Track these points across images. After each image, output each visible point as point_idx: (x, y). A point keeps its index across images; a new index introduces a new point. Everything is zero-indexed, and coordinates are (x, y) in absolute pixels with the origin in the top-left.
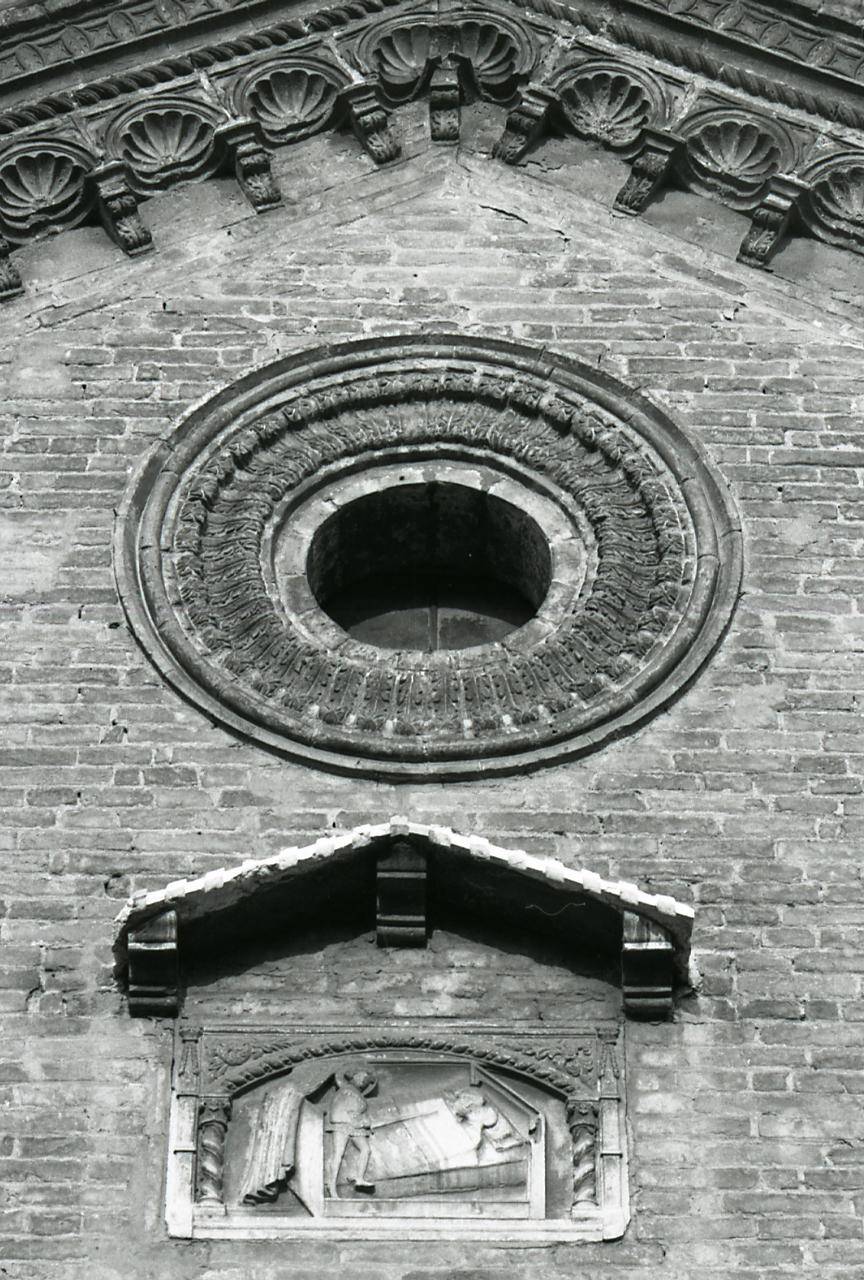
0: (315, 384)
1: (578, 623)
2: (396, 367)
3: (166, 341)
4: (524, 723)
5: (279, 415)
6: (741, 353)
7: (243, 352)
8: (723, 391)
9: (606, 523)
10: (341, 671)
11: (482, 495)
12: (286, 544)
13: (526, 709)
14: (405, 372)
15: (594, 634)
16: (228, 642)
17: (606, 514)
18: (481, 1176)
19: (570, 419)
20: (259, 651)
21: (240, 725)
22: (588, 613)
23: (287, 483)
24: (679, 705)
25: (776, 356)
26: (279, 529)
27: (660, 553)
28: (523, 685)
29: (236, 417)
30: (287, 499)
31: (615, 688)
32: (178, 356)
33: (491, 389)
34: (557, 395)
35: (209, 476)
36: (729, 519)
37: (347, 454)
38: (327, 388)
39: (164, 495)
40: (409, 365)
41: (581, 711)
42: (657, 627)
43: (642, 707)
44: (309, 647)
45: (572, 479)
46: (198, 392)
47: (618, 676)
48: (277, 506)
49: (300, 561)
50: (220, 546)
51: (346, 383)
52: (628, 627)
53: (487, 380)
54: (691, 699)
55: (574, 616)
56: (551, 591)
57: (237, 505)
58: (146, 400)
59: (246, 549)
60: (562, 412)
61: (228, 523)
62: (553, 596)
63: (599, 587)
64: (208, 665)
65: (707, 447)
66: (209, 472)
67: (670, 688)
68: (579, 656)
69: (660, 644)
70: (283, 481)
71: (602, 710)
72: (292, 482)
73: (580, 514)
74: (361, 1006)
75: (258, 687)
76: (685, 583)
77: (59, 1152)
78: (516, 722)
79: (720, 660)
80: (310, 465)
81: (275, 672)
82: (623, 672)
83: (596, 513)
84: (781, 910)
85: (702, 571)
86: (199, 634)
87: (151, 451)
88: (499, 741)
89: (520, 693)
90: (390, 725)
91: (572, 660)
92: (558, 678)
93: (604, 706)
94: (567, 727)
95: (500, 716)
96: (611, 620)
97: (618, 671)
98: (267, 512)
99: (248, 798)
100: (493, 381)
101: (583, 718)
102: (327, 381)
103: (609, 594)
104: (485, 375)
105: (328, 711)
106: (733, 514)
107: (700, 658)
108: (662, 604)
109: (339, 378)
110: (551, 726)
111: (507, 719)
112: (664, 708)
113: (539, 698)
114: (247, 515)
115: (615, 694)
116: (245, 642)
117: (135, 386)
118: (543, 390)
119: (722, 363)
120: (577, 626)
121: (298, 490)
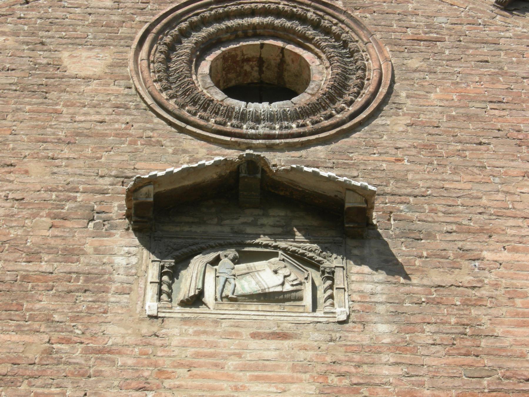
56: (311, 83)
74: (232, 229)
84: (411, 199)
99: (185, 151)
118: (308, 11)
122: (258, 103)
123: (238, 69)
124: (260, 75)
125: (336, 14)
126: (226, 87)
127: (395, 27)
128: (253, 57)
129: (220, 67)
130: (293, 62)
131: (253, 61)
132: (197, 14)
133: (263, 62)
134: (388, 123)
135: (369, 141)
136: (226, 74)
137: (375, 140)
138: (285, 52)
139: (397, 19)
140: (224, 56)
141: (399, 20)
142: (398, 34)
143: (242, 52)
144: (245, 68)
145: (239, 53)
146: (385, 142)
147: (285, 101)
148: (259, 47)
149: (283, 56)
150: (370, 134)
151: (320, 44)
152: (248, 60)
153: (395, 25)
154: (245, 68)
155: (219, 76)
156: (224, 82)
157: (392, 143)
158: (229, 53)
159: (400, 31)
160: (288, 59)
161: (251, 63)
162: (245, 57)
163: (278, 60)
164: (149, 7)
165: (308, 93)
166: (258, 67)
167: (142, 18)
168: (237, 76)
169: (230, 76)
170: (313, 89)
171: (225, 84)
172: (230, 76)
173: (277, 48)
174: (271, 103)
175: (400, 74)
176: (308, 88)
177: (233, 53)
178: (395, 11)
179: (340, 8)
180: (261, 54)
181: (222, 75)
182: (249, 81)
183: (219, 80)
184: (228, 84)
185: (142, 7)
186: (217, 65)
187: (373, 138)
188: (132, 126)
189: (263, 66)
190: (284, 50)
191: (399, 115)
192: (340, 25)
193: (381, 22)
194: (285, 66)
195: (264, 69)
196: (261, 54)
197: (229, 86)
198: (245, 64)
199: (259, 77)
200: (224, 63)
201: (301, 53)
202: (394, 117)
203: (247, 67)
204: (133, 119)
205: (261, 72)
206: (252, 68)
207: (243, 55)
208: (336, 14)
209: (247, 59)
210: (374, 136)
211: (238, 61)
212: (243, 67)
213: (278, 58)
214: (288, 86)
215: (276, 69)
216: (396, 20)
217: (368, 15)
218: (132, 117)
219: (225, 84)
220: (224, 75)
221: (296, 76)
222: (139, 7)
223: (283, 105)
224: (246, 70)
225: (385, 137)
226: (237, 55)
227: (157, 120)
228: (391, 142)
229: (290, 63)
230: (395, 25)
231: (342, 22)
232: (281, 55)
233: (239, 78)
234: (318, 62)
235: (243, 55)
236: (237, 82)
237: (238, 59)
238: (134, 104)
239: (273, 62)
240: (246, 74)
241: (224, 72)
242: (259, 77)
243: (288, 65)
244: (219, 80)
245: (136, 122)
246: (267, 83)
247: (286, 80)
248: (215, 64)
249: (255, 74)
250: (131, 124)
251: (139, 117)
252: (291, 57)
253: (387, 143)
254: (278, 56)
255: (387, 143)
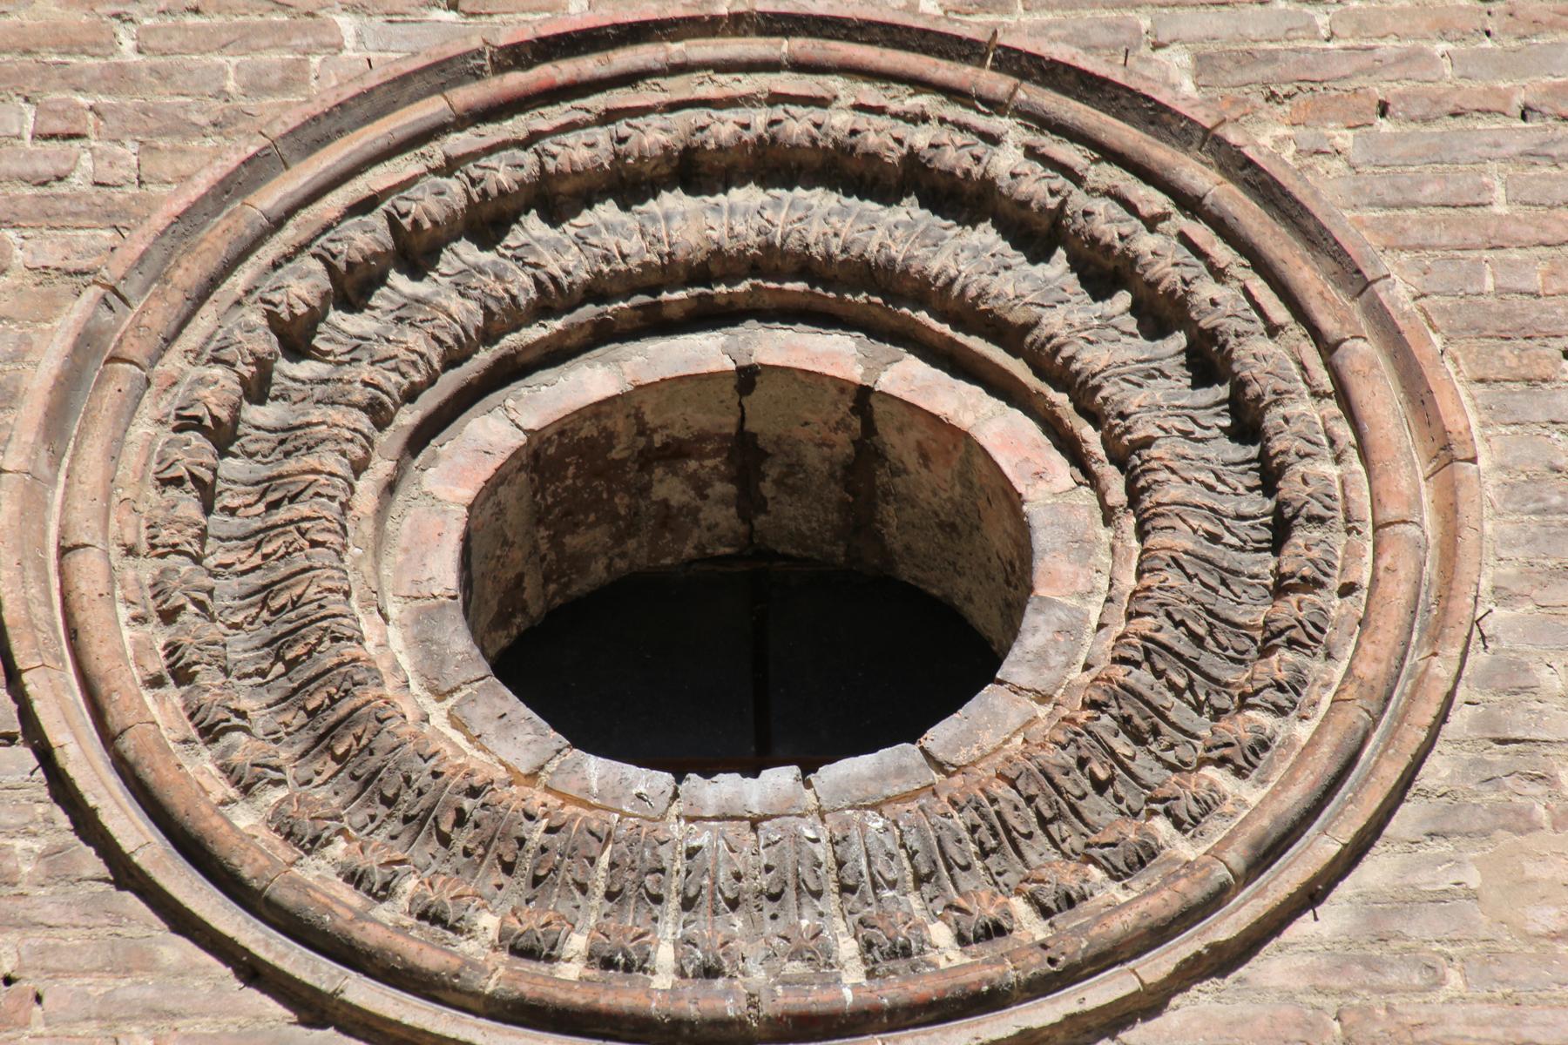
0: (458, 142)
1: (1097, 695)
2: (643, 95)
3: (103, 45)
4: (977, 940)
5: (377, 219)
6: (808, 955)
7: (285, 66)
8: (1425, 120)
9: (1154, 452)
10: (550, 830)
11: (863, 397)
12: (407, 519)
13: (985, 909)
14: (674, 107)
15: (1137, 720)
16: (278, 769)
17: (1154, 431)
18: (393, 222)
19: (1064, 203)
20: (355, 787)
21: (267, 946)
22: (1120, 672)
23: (405, 384)
24: (1345, 888)
25: (1552, 25)
26: (391, 488)
27: (1280, 530)
28: (973, 848)
29: (277, 224)
30: (408, 417)
31: (1185, 849)
32: (121, 78)
33: (872, 141)
34: (1031, 152)
35: (218, 371)
36: (1445, 432)
37: (543, 309)
38: (490, 150)
39: (118, 415)
40: (679, 88)
41: (1116, 908)
42: (1282, 700)
43: (1258, 894)
44: (470, 774)
45: (1066, 352)
46: (184, 166)
47: (1196, 821)
48: (382, 438)
49: (443, 572)
50: (255, 537)
51: (527, 142)
52: (1215, 700)
53: (862, 120)
54: (1373, 872)
55: (1087, 678)
56: (1030, 619)
57: (289, 438)
58: (59, 188)
59: (314, 544)
60: (1036, 186)
61: (265, 486)
62: (1036, 629)
63: (1144, 606)
64: (234, 828)
65: (1387, 263)
66: (216, 360)
67: (1319, 847)
68: (1102, 775)
69: (1289, 743)
70: (395, 377)
71: (1163, 903)
72: (417, 378)
73: (1091, 437)
75: (355, 878)
76: (1347, 590)
77: (931, 851)
78: (962, 940)
79: (1436, 772)
80: (457, 339)
81: (393, 838)
82: (1207, 810)
83: (1128, 430)
85: (1386, 561)
86: (206, 754)
87: (78, 309)
88: (923, 987)
89: (966, 868)
90: (665, 955)
91: (1087, 784)
92: (1053, 828)
93: (1166, 894)
94: (1076, 948)
95: (921, 926)
96: (1172, 686)
97: (1195, 809)
98: (360, 453)
100: (877, 121)
101: (1119, 925)
102: (493, 132)
103: (1168, 624)
104: (860, 108)
105: (519, 928)
106: (1453, 421)
107: (1391, 773)
108: (1292, 643)
109: (516, 126)
110: (1044, 946)
111: (941, 934)
112: (1311, 896)
113: (1011, 878)
114: (311, 461)
115: (1188, 864)
116: (317, 766)
117: (30, 156)
118: (993, 140)
119: (1420, 53)
120: (1094, 705)
121: (430, 400)
122: (735, 777)
123: (621, 502)
124: (745, 517)
125: (1160, 153)
126: (558, 601)
127: (1500, 209)
128: (702, 437)
129: (516, 515)
130: (925, 458)
131: (701, 456)
132: (365, 206)
133: (763, 455)
134: (1473, 879)
135: (1367, 1012)
136: (555, 541)
137: (1395, 1000)
138: (879, 408)
139: (1513, 149)
140: (536, 455)
141: (1531, 156)
142: (1516, 255)
143: (638, 416)
144: (660, 491)
145: (619, 424)
146: (1457, 1013)
147: (884, 753)
148: (729, 386)
149: (869, 427)
150: (1369, 964)
151: (1071, 359)
152: (674, 453)
153: (1499, 193)
154: (660, 491)
155: (517, 554)
156: (547, 579)
157: (1495, 1022)
158: (561, 433)
159: (1530, 233)
160: (899, 444)
161: (693, 464)
162: (658, 440)
163: (843, 444)
164: (86, 161)
165: (1018, 690)
166: (732, 480)
167: (51, 249)
168: (619, 539)
169: (572, 542)
170: (1041, 657)
171: (552, 587)
172: (572, 542)
173: (833, 391)
174: (809, 768)
175: (1532, 540)
176: (1016, 652)
177: (588, 430)
178: (1506, 96)
179: (1182, 108)
180: (743, 419)
181: (535, 547)
182: (689, 550)
183: (520, 577)
184: (567, 585)
185: (44, 168)
186: (500, 511)
187: (1389, 991)
188: (38, 999)
189: (762, 477)
190: (873, 400)
191: (1533, 827)
192: (1181, 222)
193: (1419, 184)
194: (882, 477)
195: (767, 488)
196: (743, 419)
197: (574, 590)
198: (659, 472)
199: (742, 529)
200: (542, 489)
201: (965, 421)
202: (1505, 839)
203: (669, 488)
204: (42, 951)
205: (749, 502)
206: (700, 487)
207: (643, 430)
208: (1160, 153)
209: (665, 446)
210: (1392, 978)
211: (622, 463)
212: (645, 490)
213: (842, 438)
214: (906, 572)
215: (835, 492)
216: (1506, 159)
217: (1344, 138)
218: (37, 938)
219: (552, 587)
220: (544, 546)
221: (950, 528)
222: (27, 168)
223: (881, 777)
224: (665, 503)
225: (1454, 978)
226: (610, 437)
227: (177, 950)
228: (1489, 1011)
229: (912, 461)
230: (1499, 193)
231: (1190, 204)
232: (856, 423)
233: (631, 544)
234: (1062, 472)
235: (642, 432)
236: (621, 564)
237: (617, 454)
238: (38, 846)
239: (812, 456)
240: (667, 516)
241: (543, 532)
242: (742, 529)
243: (899, 471)
244: (520, 577)
245: (55, 974)
246: (786, 557)
247: (897, 546)
248: (489, 509)
249: (720, 516)
250: (27, 985)
251: (73, 938)
252: (913, 436)
253: (1471, 1022)
254: (842, 425)
255: (1471, 1022)
